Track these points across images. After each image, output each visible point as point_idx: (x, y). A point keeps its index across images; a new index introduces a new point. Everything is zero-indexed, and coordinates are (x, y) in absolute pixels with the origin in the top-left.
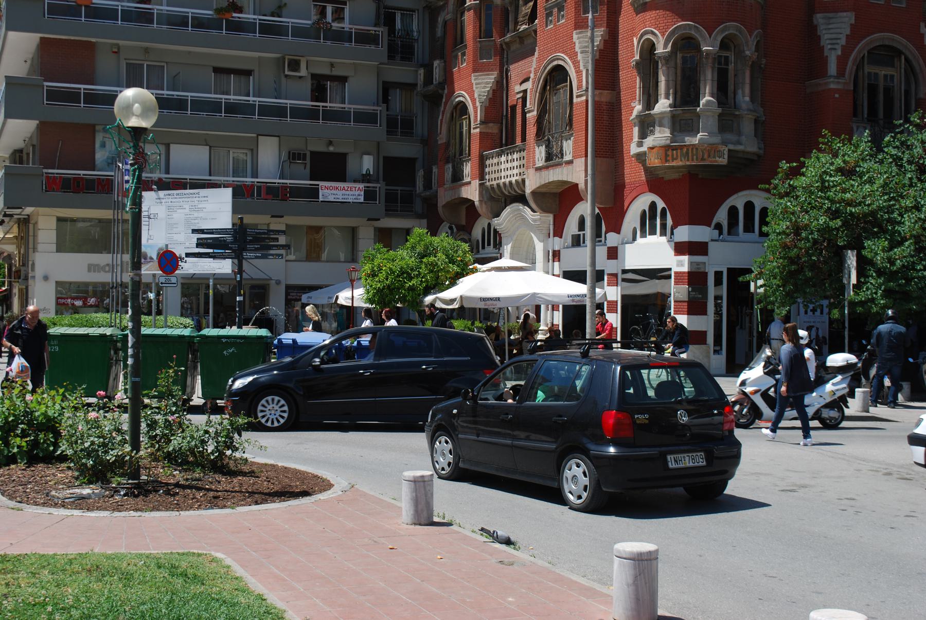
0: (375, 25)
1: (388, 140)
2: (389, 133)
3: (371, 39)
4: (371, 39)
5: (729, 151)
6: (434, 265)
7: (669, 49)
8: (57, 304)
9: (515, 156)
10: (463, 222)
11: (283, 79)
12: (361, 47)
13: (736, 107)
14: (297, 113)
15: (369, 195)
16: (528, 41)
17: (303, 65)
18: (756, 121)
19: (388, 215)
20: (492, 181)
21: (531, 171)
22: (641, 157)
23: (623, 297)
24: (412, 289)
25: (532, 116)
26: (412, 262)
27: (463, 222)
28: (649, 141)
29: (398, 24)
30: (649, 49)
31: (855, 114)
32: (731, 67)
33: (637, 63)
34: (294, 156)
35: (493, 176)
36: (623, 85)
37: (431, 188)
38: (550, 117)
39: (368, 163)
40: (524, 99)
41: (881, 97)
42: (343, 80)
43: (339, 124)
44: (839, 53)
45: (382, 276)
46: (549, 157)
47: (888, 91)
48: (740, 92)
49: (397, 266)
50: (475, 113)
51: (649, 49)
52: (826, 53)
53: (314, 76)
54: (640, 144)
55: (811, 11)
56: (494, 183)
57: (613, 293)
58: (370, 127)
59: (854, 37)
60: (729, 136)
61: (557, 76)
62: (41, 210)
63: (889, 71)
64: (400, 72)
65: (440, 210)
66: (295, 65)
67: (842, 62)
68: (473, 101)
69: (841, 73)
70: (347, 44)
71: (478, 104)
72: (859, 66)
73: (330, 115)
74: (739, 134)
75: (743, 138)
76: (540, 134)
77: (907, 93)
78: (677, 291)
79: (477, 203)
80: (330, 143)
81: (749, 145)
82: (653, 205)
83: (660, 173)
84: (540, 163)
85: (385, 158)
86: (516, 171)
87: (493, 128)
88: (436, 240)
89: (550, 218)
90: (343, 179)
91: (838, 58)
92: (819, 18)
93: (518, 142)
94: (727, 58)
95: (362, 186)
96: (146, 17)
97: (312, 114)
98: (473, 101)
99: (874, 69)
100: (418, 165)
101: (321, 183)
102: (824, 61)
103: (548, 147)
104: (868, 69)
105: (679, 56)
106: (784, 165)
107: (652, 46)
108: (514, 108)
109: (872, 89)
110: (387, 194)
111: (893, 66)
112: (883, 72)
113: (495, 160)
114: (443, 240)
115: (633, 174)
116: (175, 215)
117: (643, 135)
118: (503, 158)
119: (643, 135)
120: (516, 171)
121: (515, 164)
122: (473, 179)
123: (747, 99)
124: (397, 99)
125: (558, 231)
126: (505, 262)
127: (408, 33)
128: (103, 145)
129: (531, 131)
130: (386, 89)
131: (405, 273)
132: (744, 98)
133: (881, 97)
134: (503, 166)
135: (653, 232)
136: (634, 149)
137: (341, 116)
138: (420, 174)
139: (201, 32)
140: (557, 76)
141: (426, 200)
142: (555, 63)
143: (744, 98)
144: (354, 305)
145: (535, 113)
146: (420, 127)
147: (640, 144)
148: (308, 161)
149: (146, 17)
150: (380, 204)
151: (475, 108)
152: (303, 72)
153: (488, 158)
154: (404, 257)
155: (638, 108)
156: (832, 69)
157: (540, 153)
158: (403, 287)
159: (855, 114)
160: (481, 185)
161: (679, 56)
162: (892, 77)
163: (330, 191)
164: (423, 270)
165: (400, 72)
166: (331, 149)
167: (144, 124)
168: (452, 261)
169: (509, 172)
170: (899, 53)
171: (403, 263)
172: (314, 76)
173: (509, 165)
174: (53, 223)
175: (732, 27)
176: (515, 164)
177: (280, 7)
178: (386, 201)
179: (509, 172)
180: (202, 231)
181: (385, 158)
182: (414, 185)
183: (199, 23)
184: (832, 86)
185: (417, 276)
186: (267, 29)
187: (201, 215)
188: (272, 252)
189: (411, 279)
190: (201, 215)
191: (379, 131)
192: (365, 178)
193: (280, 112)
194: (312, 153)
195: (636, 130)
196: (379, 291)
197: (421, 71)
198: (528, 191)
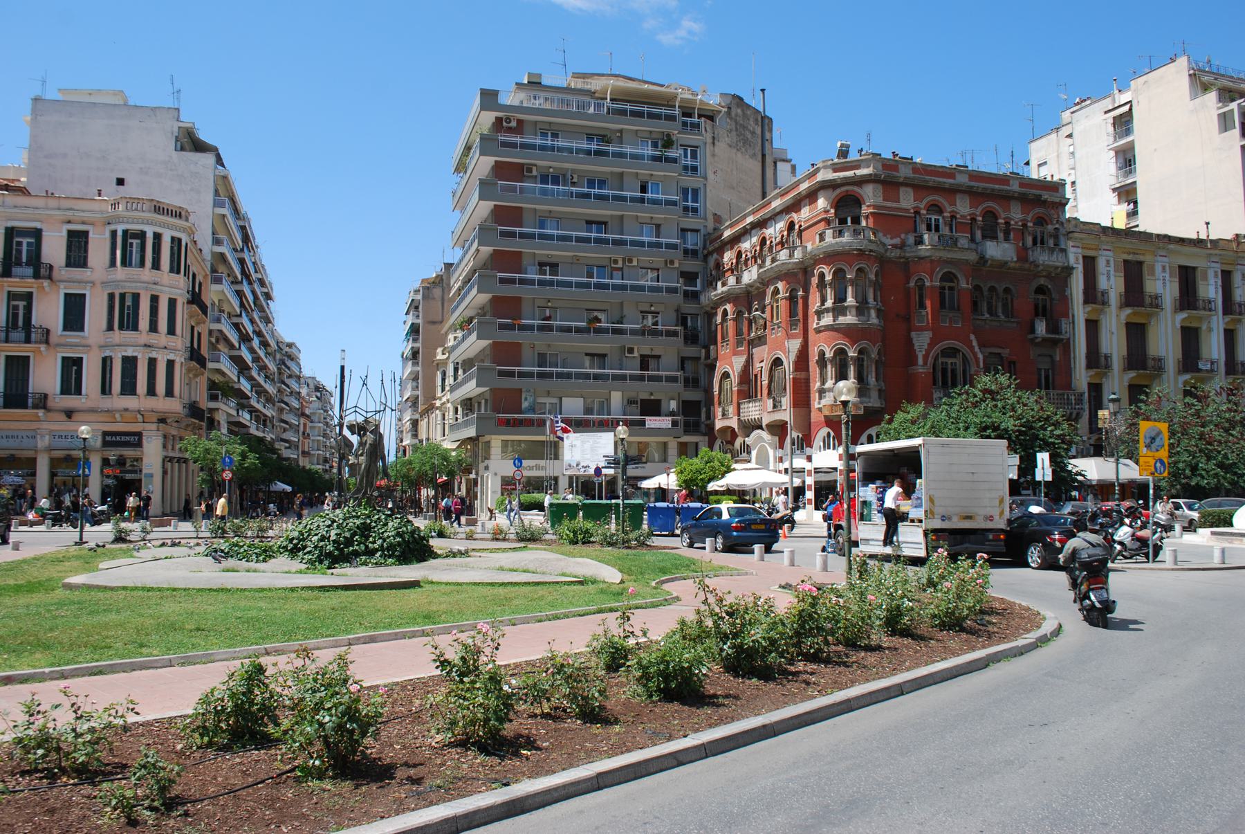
0: (676, 326)
1: (685, 391)
2: (685, 386)
3: (675, 334)
4: (675, 334)
5: (865, 407)
6: (713, 467)
7: (832, 355)
8: (502, 488)
9: (757, 404)
10: (729, 439)
11: (624, 359)
12: (668, 339)
13: (868, 384)
14: (633, 378)
15: (674, 424)
16: (763, 340)
17: (636, 350)
18: (880, 391)
19: (685, 435)
20: (744, 417)
21: (765, 413)
22: (820, 409)
23: (815, 482)
24: (702, 480)
25: (765, 383)
26: (702, 466)
27: (729, 439)
28: (824, 402)
29: (689, 323)
30: (822, 354)
31: (934, 384)
32: (865, 363)
33: (817, 362)
34: (631, 402)
35: (745, 414)
36: (811, 369)
37: (710, 419)
38: (774, 384)
39: (673, 405)
40: (761, 371)
41: (949, 374)
42: (659, 357)
43: (656, 384)
44: (924, 353)
45: (686, 474)
46: (775, 406)
47: (953, 371)
48: (870, 376)
49: (693, 468)
50: (734, 379)
51: (822, 354)
52: (917, 353)
53: (641, 356)
54: (819, 403)
55: (909, 331)
56: (746, 418)
57: (810, 481)
58: (674, 384)
59: (932, 344)
60: (864, 399)
61: (777, 362)
62: (493, 437)
63: (953, 360)
64: (691, 351)
65: (716, 432)
66: (631, 350)
67: (926, 357)
68: (733, 372)
69: (925, 363)
70: (660, 338)
71: (736, 374)
72: (936, 359)
73: (651, 379)
74: (870, 397)
75: (872, 400)
76: (769, 393)
77: (964, 371)
78: (840, 479)
79: (736, 430)
80: (652, 394)
81: (874, 402)
82: (829, 434)
83: (831, 418)
84: (770, 409)
85: (683, 401)
86: (757, 413)
87: (745, 387)
88: (714, 453)
89: (777, 438)
90: (659, 415)
91: (923, 355)
92: (913, 334)
93: (759, 397)
94: (863, 359)
95: (670, 418)
96: (549, 329)
97: (641, 378)
98: (733, 372)
99: (945, 360)
100: (703, 404)
101: (647, 418)
102: (916, 357)
103: (774, 400)
104: (940, 360)
105: (838, 358)
106: (887, 417)
107: (824, 354)
108: (756, 376)
109: (944, 371)
110: (684, 422)
111: (955, 357)
112: (950, 361)
113: (746, 406)
114: (717, 453)
115: (815, 417)
116: (585, 445)
117: (820, 398)
118: (751, 405)
119: (820, 398)
120: (757, 413)
121: (757, 408)
122: (734, 415)
123: (874, 379)
124: (689, 366)
125: (781, 446)
126: (753, 465)
127: (695, 328)
128: (526, 399)
129: (765, 392)
130: (683, 361)
131: (699, 472)
132: (872, 380)
133: (949, 374)
134: (750, 409)
135: (829, 448)
136: (817, 406)
137: (658, 379)
138: (704, 410)
139: (579, 335)
140: (777, 362)
141: (707, 425)
142: (776, 356)
143: (872, 380)
144: (1111, 574)
145: (767, 382)
146: (703, 382)
147: (819, 403)
148: (639, 405)
149: (549, 329)
150: (681, 428)
151: (734, 376)
152: (636, 354)
153: (742, 403)
154: (697, 463)
155: (818, 384)
156: (920, 361)
157: (770, 403)
158: (697, 478)
159: (934, 384)
160: (739, 419)
161: (838, 358)
162: (955, 363)
163: (652, 422)
164: (707, 470)
165: (691, 351)
166: (652, 398)
167: (624, 437)
168: (722, 465)
169: (754, 413)
170: (959, 351)
171: (697, 466)
172: (641, 356)
173: (754, 409)
174: (499, 444)
175: (864, 344)
176: (757, 408)
177: (622, 317)
178: (685, 426)
179: (754, 413)
180: (608, 456)
181: (683, 401)
182: (700, 417)
183: (578, 330)
184: (921, 371)
185: (705, 473)
186: (616, 332)
187: (598, 445)
188: (197, 290)
189: (701, 474)
190: (598, 445)
191: (679, 386)
192: (672, 414)
193: (623, 378)
194: (641, 400)
195: (817, 395)
196: (685, 481)
197: (703, 351)
198: (764, 425)
